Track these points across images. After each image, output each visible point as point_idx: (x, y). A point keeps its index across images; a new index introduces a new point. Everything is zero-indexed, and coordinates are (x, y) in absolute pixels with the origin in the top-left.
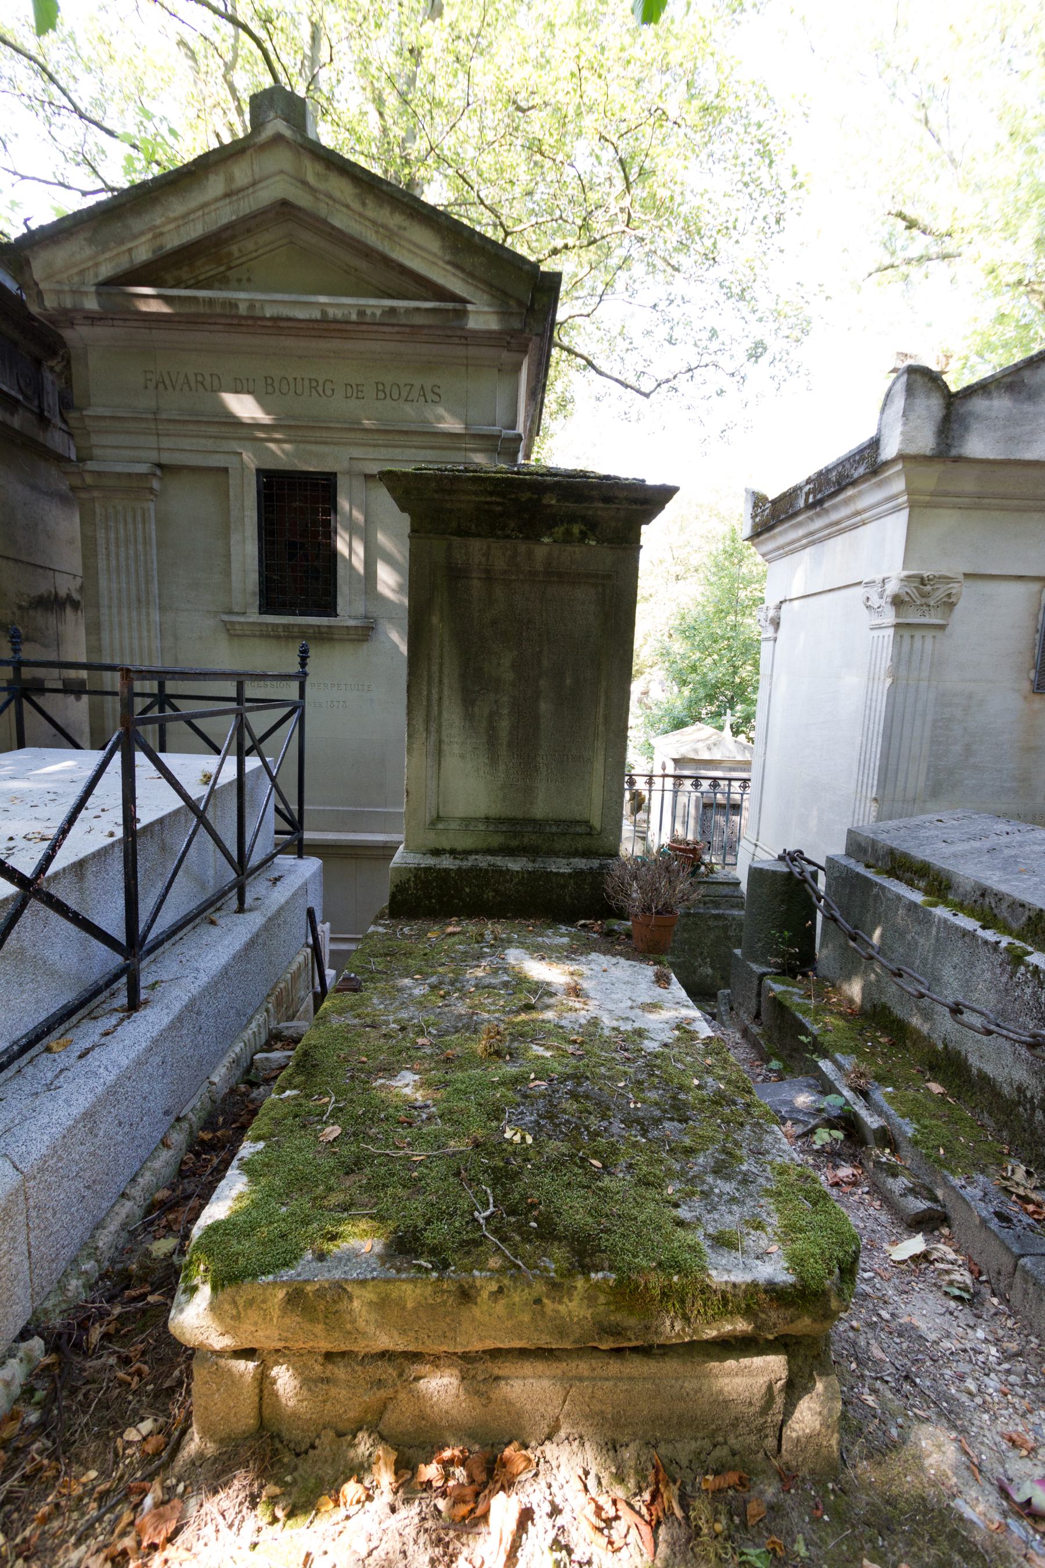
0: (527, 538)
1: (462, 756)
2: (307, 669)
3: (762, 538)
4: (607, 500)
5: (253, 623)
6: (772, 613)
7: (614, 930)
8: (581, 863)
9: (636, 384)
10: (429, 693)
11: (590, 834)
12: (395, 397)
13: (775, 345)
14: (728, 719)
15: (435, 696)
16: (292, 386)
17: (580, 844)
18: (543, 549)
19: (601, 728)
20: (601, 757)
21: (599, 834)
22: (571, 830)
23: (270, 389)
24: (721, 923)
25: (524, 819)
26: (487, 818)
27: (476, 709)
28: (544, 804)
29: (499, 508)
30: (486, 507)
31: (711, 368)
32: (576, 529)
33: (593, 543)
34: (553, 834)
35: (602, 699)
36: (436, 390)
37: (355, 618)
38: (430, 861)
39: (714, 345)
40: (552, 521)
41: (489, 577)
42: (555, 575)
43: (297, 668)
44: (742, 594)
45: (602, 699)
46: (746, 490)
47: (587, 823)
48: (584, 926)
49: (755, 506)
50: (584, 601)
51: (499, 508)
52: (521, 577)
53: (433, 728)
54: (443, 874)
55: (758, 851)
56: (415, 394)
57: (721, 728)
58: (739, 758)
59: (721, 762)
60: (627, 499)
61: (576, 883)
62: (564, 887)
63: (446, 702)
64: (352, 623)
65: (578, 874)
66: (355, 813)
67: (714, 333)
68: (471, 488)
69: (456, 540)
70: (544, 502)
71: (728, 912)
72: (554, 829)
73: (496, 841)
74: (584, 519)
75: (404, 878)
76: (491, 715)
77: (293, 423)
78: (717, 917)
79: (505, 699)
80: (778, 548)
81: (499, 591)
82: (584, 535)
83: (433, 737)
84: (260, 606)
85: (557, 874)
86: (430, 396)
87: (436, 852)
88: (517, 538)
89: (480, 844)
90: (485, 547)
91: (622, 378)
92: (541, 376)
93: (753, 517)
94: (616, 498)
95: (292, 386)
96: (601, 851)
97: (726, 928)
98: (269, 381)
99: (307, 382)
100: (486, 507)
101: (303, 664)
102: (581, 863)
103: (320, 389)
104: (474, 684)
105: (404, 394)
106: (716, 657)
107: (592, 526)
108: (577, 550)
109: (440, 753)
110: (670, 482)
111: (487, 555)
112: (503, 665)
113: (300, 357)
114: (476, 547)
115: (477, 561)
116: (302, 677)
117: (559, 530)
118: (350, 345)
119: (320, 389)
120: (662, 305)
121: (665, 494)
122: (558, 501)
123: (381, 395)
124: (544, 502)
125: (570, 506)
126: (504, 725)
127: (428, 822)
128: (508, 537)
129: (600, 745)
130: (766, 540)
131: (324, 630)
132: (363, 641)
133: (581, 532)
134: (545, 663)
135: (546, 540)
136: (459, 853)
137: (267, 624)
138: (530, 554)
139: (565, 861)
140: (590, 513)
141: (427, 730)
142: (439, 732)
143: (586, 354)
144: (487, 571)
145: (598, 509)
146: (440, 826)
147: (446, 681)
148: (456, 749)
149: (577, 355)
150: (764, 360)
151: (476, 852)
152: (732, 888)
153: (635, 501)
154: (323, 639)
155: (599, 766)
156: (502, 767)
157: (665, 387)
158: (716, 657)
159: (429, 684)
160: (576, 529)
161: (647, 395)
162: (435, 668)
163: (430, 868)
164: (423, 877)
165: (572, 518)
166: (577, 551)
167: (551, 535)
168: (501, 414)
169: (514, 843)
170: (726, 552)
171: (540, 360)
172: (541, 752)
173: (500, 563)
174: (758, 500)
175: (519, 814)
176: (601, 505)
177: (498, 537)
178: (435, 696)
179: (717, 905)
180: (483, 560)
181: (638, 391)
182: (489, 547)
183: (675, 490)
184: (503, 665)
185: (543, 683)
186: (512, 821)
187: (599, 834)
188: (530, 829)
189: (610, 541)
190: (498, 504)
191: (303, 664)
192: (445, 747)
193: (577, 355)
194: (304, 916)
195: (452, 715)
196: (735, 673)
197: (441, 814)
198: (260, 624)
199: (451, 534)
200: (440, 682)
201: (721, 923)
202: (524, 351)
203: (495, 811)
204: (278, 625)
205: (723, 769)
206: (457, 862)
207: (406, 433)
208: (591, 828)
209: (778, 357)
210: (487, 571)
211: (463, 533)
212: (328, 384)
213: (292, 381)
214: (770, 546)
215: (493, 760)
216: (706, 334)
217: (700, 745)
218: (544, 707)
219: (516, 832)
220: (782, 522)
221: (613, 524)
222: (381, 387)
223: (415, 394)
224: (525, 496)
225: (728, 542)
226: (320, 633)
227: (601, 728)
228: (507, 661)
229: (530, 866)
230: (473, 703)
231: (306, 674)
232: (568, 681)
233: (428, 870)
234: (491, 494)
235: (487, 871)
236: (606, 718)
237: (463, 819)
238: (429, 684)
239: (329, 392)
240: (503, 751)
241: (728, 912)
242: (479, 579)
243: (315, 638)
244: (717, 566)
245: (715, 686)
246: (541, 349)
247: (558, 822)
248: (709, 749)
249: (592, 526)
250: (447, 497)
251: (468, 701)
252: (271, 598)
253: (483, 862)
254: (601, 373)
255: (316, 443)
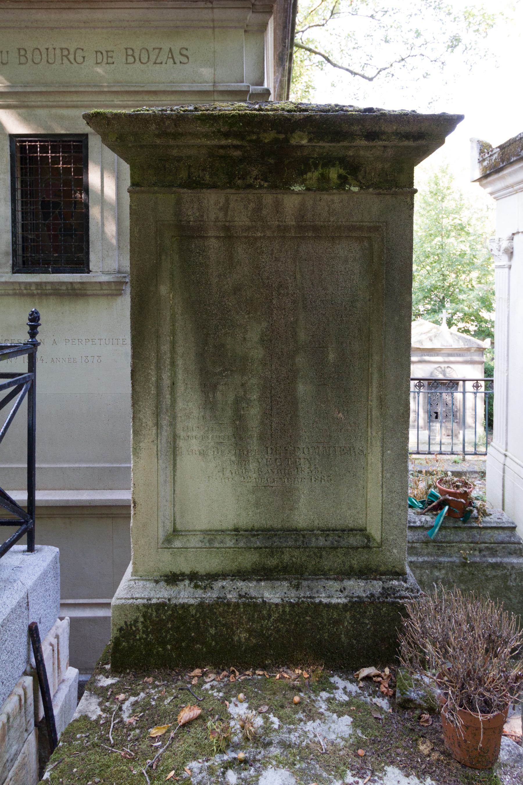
0: (274, 187)
1: (203, 454)
2: (38, 338)
3: (490, 179)
4: (372, 136)
5: (6, 283)
6: (505, 244)
7: (410, 701)
8: (358, 588)
9: (362, 73)
10: (159, 378)
11: (367, 547)
12: (144, 60)
13: (466, 38)
14: (444, 315)
15: (166, 382)
16: (44, 56)
17: (356, 561)
18: (294, 199)
19: (375, 413)
20: (377, 449)
21: (380, 546)
22: (343, 543)
23: (23, 60)
24: (499, 573)
25: (283, 530)
26: (236, 530)
27: (218, 394)
28: (307, 511)
29: (237, 153)
30: (222, 152)
31: (419, 57)
32: (333, 174)
33: (356, 189)
34: (320, 548)
35: (376, 376)
36: (184, 52)
37: (108, 273)
38: (162, 593)
39: (421, 41)
40: (303, 165)
41: (228, 234)
42: (308, 229)
43: (24, 337)
44: (445, 222)
45: (376, 376)
46: (471, 140)
47: (362, 530)
48: (368, 678)
49: (481, 152)
50: (347, 261)
51: (237, 153)
52: (268, 233)
53: (165, 421)
54: (178, 613)
55: (508, 462)
56: (163, 57)
57: (437, 322)
58: (455, 346)
59: (441, 350)
60: (397, 134)
61: (353, 617)
62: (337, 622)
63: (181, 388)
64: (104, 278)
65: (356, 605)
66: (111, 470)
67: (418, 34)
68: (206, 129)
69: (187, 194)
70: (293, 142)
71: (506, 560)
72: (322, 542)
73: (248, 560)
74: (342, 161)
75: (130, 619)
76: (237, 401)
77: (44, 89)
78: (495, 566)
79: (254, 381)
80: (507, 187)
81: (241, 252)
82: (343, 181)
83: (166, 432)
84: (14, 266)
85: (328, 606)
86: (178, 58)
87: (172, 579)
88: (261, 187)
89: (230, 565)
90: (222, 200)
91: (351, 68)
92: (288, 41)
93: (481, 162)
94: (384, 133)
95: (44, 56)
96: (383, 568)
97: (505, 578)
98: (22, 52)
99: (58, 52)
100: (222, 152)
101: (33, 333)
102: (358, 588)
103: (71, 57)
104: (214, 366)
105: (153, 57)
106: (428, 268)
107: (352, 169)
108: (336, 198)
109: (174, 451)
110: (451, 111)
111: (225, 209)
112: (250, 339)
113: (52, 29)
114: (212, 200)
115: (213, 217)
116: (30, 350)
117: (313, 176)
118: (98, 15)
119: (71, 57)
120: (378, 16)
121: (460, 118)
122: (310, 140)
123: (130, 59)
124: (293, 142)
125: (326, 146)
126: (254, 413)
127: (161, 535)
128: (250, 186)
129: (375, 433)
130: (494, 180)
131: (77, 286)
132: (117, 295)
133: (340, 176)
134: (302, 336)
135: (297, 188)
136: (202, 578)
137: (20, 283)
138: (278, 207)
139: (337, 585)
140: (351, 153)
141: (157, 425)
142: (173, 424)
143: (323, 52)
144: (227, 228)
145: (360, 148)
146: (177, 544)
147: (180, 362)
148: (195, 445)
149: (316, 53)
150: (460, 47)
151: (224, 576)
152: (508, 532)
153: (407, 136)
154: (77, 295)
155: (374, 458)
156: (253, 466)
157: (383, 73)
158: (428, 268)
159: (158, 369)
160: (333, 174)
161: (371, 79)
162: (165, 348)
163: (163, 605)
164: (156, 616)
165: (328, 161)
166: (335, 200)
167: (303, 182)
168: (248, 72)
169: (272, 562)
170: (431, 192)
171: (285, 23)
172: (302, 445)
173: (241, 218)
174: (484, 148)
175: (277, 523)
176: (364, 143)
177: (238, 188)
178: (166, 382)
179: (493, 553)
180: (221, 215)
181: (363, 77)
182: (227, 200)
183: (460, 118)
184: (250, 339)
185: (300, 360)
186: (267, 532)
187: (380, 546)
188: (291, 543)
189: (376, 186)
190: (236, 147)
191: (33, 333)
192: (181, 443)
193: (316, 53)
194: (24, 638)
195: (189, 404)
196: (444, 280)
197: (179, 527)
198: (13, 283)
199: (181, 186)
200: (173, 363)
201: (499, 573)
202: (270, 13)
203: (247, 518)
204: (30, 284)
205: (443, 355)
206: (199, 593)
207: (155, 93)
208: (369, 538)
209: (469, 47)
210: (227, 228)
211: (194, 184)
212: (79, 52)
213: (44, 51)
214: (499, 185)
215: (242, 455)
216: (413, 34)
217: (424, 337)
218: (303, 389)
219: (276, 549)
220: (511, 164)
221: (379, 166)
222: (130, 52)
223: (163, 57)
224: (268, 137)
225: (433, 185)
226: (74, 289)
227: (375, 413)
228: (254, 335)
229: (293, 596)
230: (214, 387)
231: (35, 345)
232: (332, 356)
233: (160, 606)
234: (226, 135)
235: (237, 605)
236: (381, 401)
237: (205, 532)
238: (158, 369)
239: (80, 59)
240: (254, 445)
241: (506, 560)
242: (217, 237)
243: (69, 295)
244: (425, 202)
245: (430, 291)
246: (286, 11)
247: (326, 531)
248: (431, 340)
249: (352, 169)
250: (172, 142)
251: (208, 385)
252: (28, 255)
253: (231, 591)
254: (335, 65)
255: (68, 107)
